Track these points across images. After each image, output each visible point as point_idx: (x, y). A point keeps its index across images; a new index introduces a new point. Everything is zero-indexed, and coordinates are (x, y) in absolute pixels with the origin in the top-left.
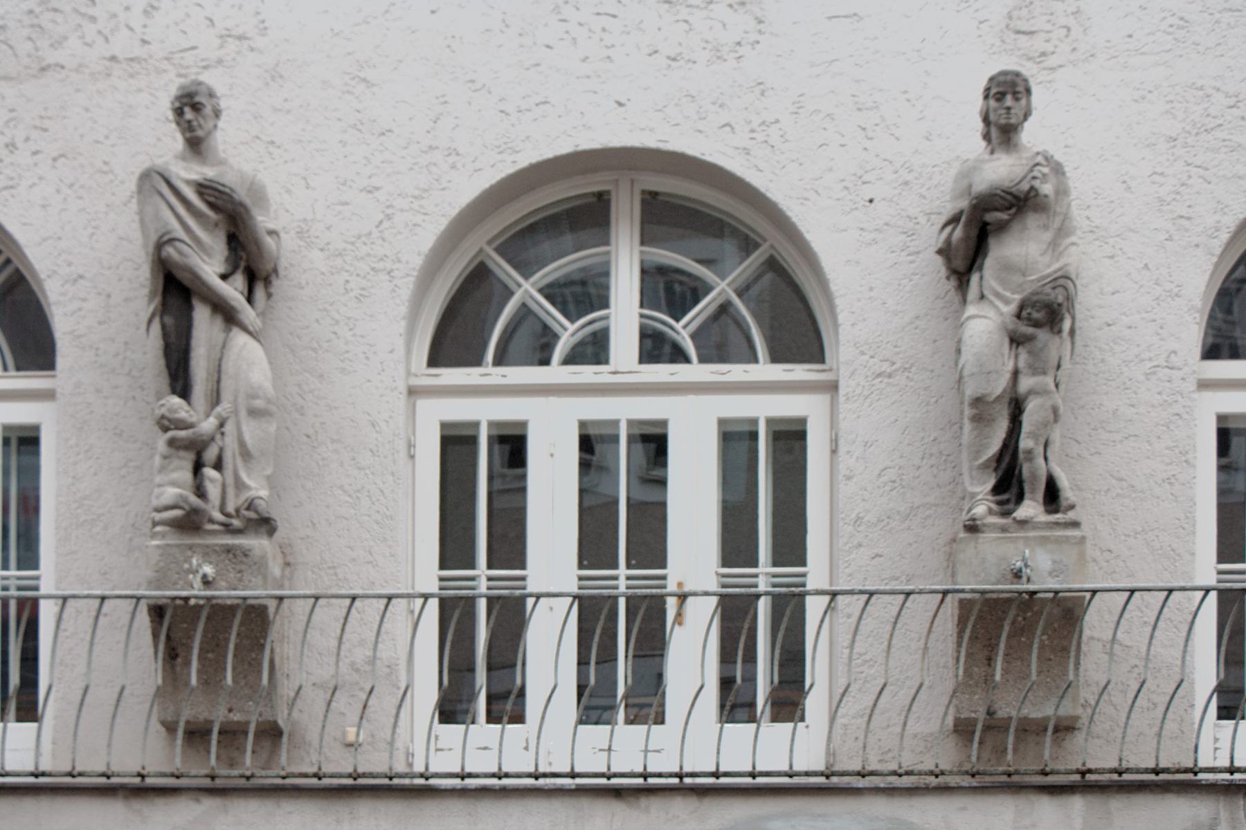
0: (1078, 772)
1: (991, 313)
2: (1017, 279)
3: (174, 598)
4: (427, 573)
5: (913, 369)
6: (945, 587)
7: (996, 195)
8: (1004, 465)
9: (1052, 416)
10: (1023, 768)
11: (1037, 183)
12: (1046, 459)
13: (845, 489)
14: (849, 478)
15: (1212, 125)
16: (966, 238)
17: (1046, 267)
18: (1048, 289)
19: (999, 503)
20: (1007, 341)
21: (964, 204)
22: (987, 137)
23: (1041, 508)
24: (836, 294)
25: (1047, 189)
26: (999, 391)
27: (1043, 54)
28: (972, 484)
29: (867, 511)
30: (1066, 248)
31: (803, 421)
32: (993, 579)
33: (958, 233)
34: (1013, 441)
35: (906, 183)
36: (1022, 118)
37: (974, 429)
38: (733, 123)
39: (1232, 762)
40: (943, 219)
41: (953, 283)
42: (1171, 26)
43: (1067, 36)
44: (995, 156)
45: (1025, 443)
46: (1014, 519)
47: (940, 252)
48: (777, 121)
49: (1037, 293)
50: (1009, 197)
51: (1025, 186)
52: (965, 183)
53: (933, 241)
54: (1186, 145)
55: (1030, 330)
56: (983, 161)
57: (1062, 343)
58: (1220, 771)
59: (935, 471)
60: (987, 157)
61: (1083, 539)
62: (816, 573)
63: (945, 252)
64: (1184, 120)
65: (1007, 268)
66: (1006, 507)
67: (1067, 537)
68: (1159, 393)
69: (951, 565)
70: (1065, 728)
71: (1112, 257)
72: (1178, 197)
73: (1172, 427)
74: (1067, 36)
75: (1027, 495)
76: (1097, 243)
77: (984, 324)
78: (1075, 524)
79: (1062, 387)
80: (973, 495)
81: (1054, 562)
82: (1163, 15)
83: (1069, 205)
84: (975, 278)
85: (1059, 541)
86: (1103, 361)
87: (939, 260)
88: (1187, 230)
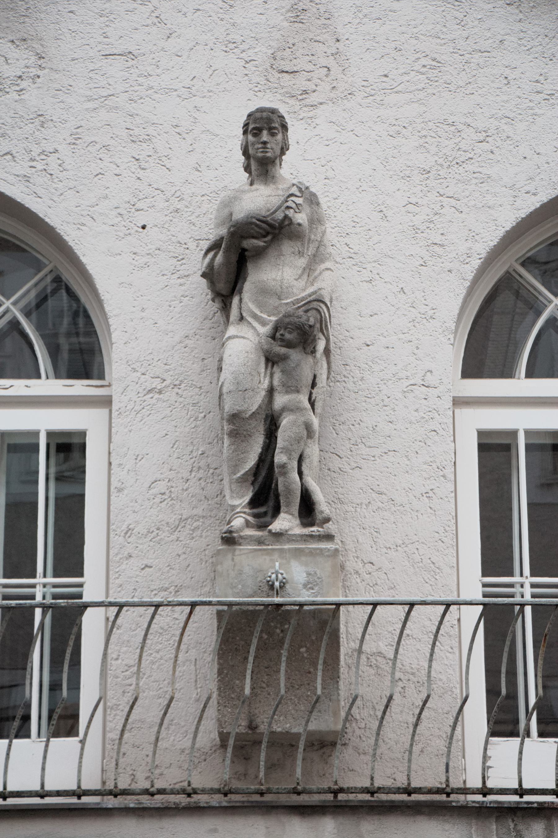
0: (330, 791)
1: (249, 334)
2: (273, 302)
3: (266, 605)
4: (472, 583)
5: (182, 386)
6: (193, 599)
7: (252, 223)
8: (260, 479)
9: (305, 433)
10: (275, 787)
11: (290, 213)
12: (300, 473)
13: (117, 501)
14: (120, 490)
15: (462, 159)
16: (227, 262)
17: (300, 290)
18: (301, 312)
19: (255, 516)
20: (263, 360)
21: (223, 231)
22: (247, 169)
23: (297, 521)
24: (109, 314)
25: (301, 218)
26: (254, 408)
27: (305, 92)
28: (232, 497)
29: (137, 522)
30: (320, 273)
31: (83, 434)
32: (250, 591)
33: (219, 258)
34: (269, 457)
35: (177, 211)
36: (278, 152)
37: (232, 444)
38: (14, 152)
39: (484, 783)
40: (205, 245)
41: (216, 306)
42: (424, 66)
43: (327, 76)
44: (255, 187)
45: (280, 458)
46: (270, 531)
47: (204, 275)
48: (56, 151)
49: (289, 316)
50: (264, 225)
51: (280, 215)
52: (226, 211)
53: (199, 266)
54: (438, 177)
55: (283, 350)
56: (243, 192)
57: (316, 363)
58: (474, 792)
59: (203, 484)
60: (247, 187)
61: (337, 550)
62: (92, 585)
63: (209, 275)
64: (436, 154)
65: (264, 291)
66: (262, 520)
67: (321, 550)
68: (417, 410)
69: (214, 575)
70: (324, 745)
71: (370, 281)
72: (432, 225)
73: (429, 442)
74: (327, 76)
75: (282, 508)
76: (356, 268)
77: (243, 344)
78: (329, 537)
79: (318, 405)
80: (233, 507)
81: (309, 574)
82: (418, 55)
83: (324, 233)
84: (235, 300)
85: (313, 553)
86: (362, 379)
87: (204, 281)
88: (440, 257)
